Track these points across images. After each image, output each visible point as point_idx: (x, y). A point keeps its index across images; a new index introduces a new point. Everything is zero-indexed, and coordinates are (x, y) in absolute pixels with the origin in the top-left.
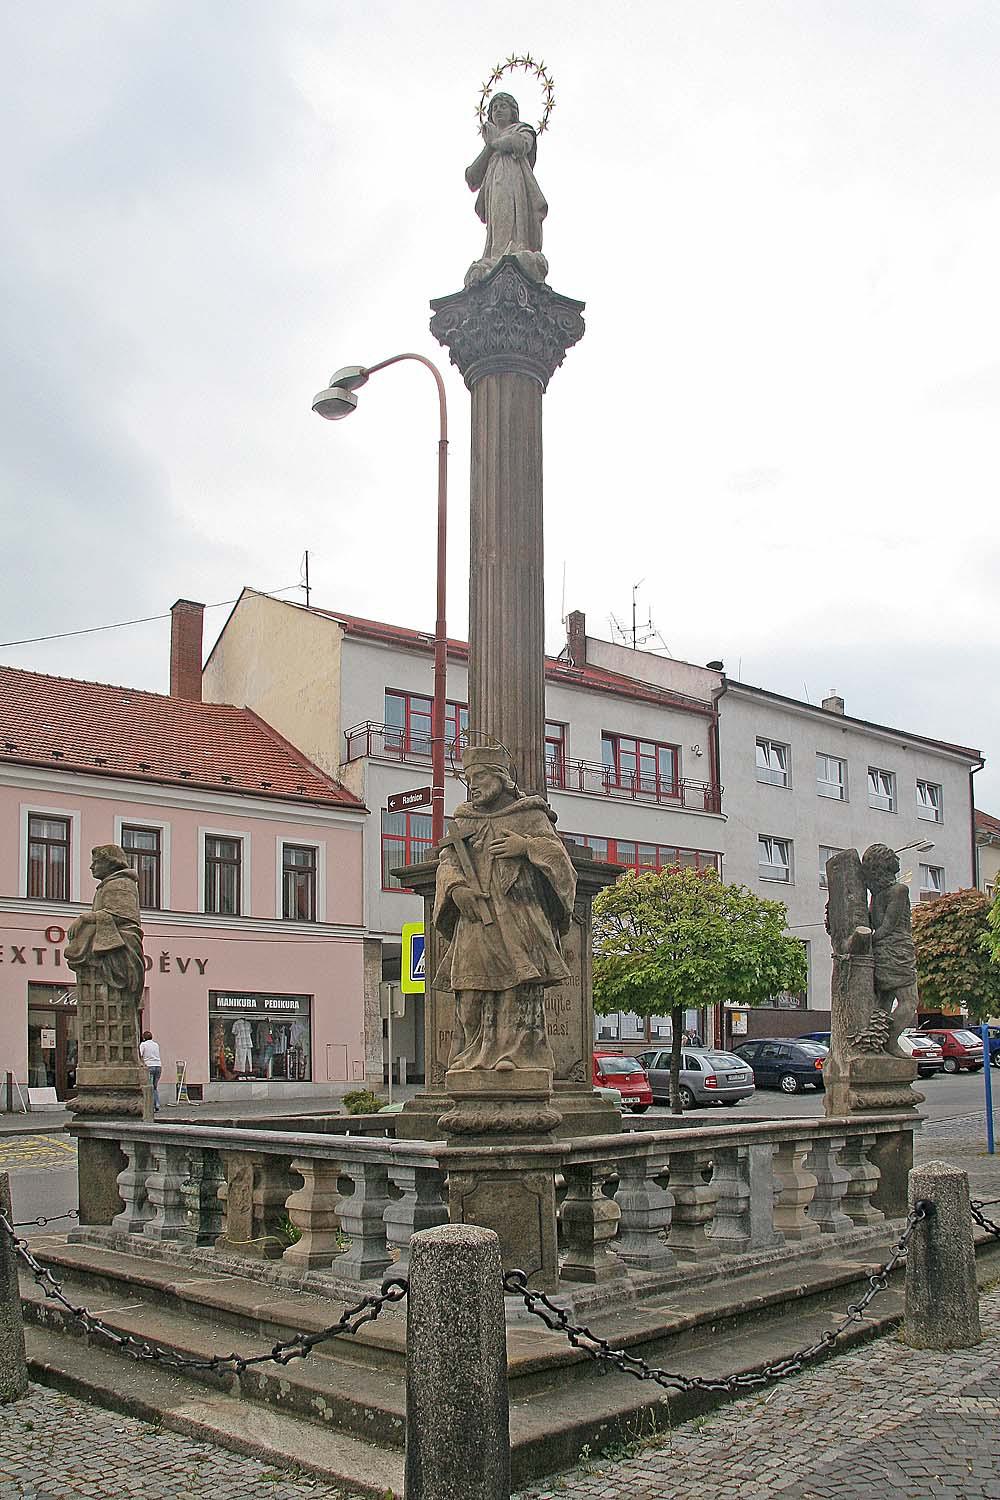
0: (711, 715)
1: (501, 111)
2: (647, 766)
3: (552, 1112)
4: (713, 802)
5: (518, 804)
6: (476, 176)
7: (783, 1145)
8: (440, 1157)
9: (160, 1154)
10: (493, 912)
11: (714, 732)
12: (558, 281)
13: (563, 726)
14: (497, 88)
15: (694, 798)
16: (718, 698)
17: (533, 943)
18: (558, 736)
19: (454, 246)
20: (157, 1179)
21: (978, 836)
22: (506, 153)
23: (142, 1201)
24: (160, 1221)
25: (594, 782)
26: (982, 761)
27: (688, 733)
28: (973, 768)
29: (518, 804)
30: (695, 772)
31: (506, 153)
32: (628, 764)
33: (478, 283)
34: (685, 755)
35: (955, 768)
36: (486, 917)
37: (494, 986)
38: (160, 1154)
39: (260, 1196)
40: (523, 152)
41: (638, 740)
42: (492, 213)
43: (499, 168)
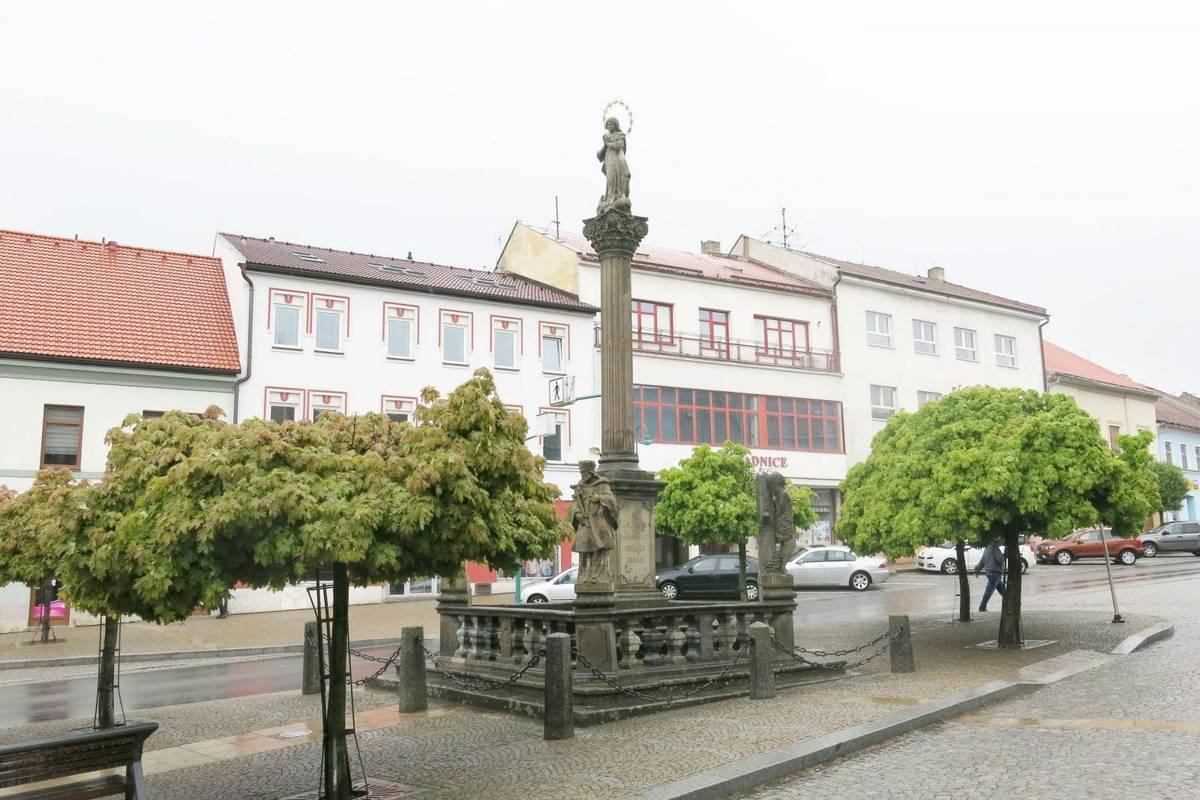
0: (830, 298)
1: (613, 126)
2: (787, 339)
3: (611, 599)
4: (834, 365)
5: (597, 481)
6: (602, 156)
7: (774, 613)
8: (573, 617)
9: (475, 620)
10: (589, 523)
11: (834, 309)
12: (636, 211)
13: (727, 313)
14: (608, 116)
15: (822, 362)
16: (835, 285)
17: (603, 535)
18: (723, 320)
19: (588, 196)
20: (474, 632)
21: (1049, 377)
22: (613, 145)
23: (467, 644)
24: (474, 651)
25: (748, 354)
26: (1047, 316)
27: (815, 311)
28: (1042, 322)
29: (597, 481)
30: (821, 341)
31: (613, 145)
32: (773, 338)
33: (603, 216)
34: (812, 328)
35: (1027, 324)
36: (587, 525)
37: (590, 550)
38: (475, 620)
39: (514, 635)
40: (620, 148)
41: (779, 320)
42: (608, 171)
43: (609, 155)
